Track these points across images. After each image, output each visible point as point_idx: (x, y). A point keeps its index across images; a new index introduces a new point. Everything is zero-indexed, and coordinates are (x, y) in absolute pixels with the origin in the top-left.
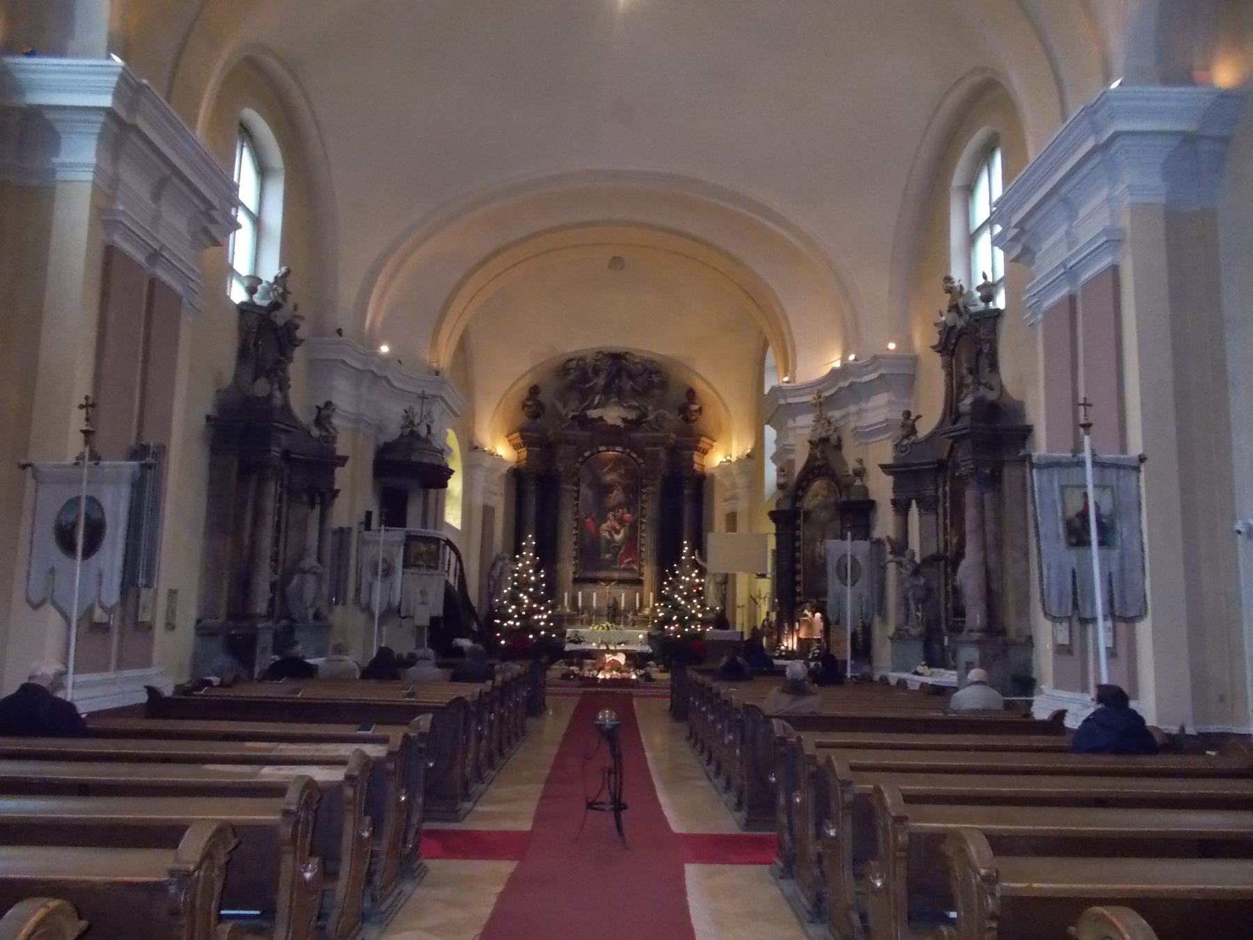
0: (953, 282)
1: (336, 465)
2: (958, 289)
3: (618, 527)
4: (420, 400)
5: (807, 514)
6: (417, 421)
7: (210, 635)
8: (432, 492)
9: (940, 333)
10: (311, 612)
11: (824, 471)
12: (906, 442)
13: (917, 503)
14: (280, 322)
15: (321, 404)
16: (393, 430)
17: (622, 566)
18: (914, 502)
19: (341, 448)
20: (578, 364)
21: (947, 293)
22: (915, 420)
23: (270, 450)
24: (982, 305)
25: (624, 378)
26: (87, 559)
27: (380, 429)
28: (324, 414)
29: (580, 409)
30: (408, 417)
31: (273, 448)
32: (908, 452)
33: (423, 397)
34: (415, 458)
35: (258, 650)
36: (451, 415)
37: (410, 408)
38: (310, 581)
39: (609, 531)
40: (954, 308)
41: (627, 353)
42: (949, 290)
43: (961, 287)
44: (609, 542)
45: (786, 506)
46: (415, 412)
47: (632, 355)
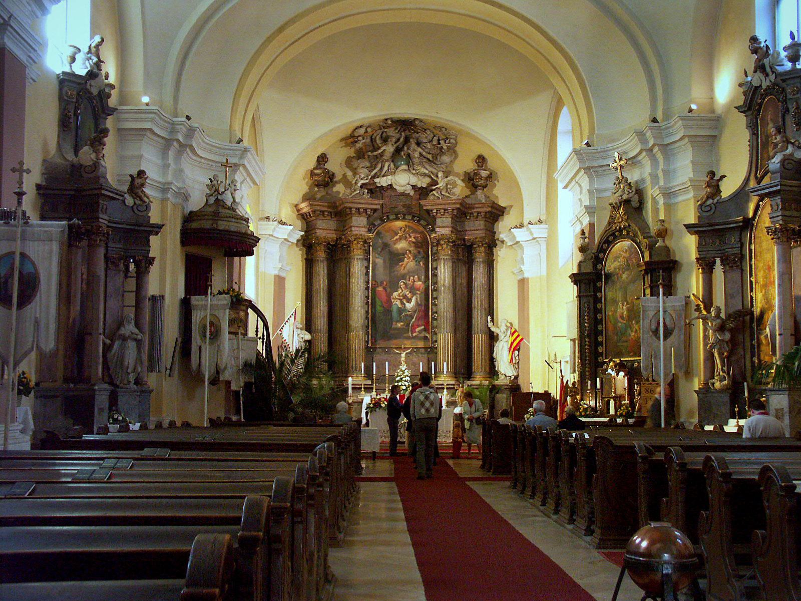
0: (760, 43)
1: (151, 233)
2: (765, 49)
3: (409, 296)
4: (224, 168)
5: (608, 276)
6: (221, 190)
7: (46, 397)
8: (236, 259)
9: (745, 93)
10: (132, 378)
11: (624, 232)
12: (710, 202)
13: (722, 261)
14: (95, 92)
15: (134, 172)
16: (197, 202)
17: (414, 335)
18: (718, 261)
19: (155, 217)
20: (366, 132)
21: (753, 54)
22: (719, 180)
23: (98, 218)
24: (788, 65)
25: (413, 145)
26: (20, 309)
27: (186, 197)
28: (137, 181)
29: (370, 177)
30: (213, 186)
31: (101, 216)
32: (713, 211)
33: (226, 165)
34: (222, 225)
35: (96, 410)
36: (251, 184)
37: (215, 176)
38: (131, 345)
39: (399, 299)
40: (760, 68)
41: (415, 119)
42: (755, 51)
43: (767, 47)
44: (400, 311)
45: (589, 268)
46: (220, 180)
47: (421, 121)
